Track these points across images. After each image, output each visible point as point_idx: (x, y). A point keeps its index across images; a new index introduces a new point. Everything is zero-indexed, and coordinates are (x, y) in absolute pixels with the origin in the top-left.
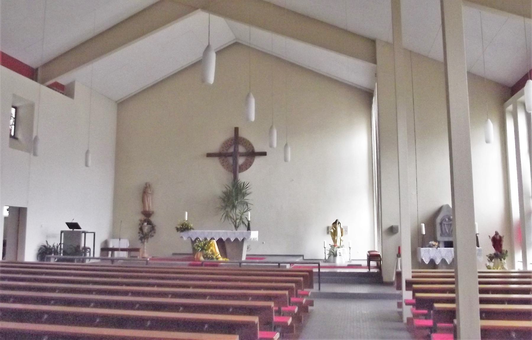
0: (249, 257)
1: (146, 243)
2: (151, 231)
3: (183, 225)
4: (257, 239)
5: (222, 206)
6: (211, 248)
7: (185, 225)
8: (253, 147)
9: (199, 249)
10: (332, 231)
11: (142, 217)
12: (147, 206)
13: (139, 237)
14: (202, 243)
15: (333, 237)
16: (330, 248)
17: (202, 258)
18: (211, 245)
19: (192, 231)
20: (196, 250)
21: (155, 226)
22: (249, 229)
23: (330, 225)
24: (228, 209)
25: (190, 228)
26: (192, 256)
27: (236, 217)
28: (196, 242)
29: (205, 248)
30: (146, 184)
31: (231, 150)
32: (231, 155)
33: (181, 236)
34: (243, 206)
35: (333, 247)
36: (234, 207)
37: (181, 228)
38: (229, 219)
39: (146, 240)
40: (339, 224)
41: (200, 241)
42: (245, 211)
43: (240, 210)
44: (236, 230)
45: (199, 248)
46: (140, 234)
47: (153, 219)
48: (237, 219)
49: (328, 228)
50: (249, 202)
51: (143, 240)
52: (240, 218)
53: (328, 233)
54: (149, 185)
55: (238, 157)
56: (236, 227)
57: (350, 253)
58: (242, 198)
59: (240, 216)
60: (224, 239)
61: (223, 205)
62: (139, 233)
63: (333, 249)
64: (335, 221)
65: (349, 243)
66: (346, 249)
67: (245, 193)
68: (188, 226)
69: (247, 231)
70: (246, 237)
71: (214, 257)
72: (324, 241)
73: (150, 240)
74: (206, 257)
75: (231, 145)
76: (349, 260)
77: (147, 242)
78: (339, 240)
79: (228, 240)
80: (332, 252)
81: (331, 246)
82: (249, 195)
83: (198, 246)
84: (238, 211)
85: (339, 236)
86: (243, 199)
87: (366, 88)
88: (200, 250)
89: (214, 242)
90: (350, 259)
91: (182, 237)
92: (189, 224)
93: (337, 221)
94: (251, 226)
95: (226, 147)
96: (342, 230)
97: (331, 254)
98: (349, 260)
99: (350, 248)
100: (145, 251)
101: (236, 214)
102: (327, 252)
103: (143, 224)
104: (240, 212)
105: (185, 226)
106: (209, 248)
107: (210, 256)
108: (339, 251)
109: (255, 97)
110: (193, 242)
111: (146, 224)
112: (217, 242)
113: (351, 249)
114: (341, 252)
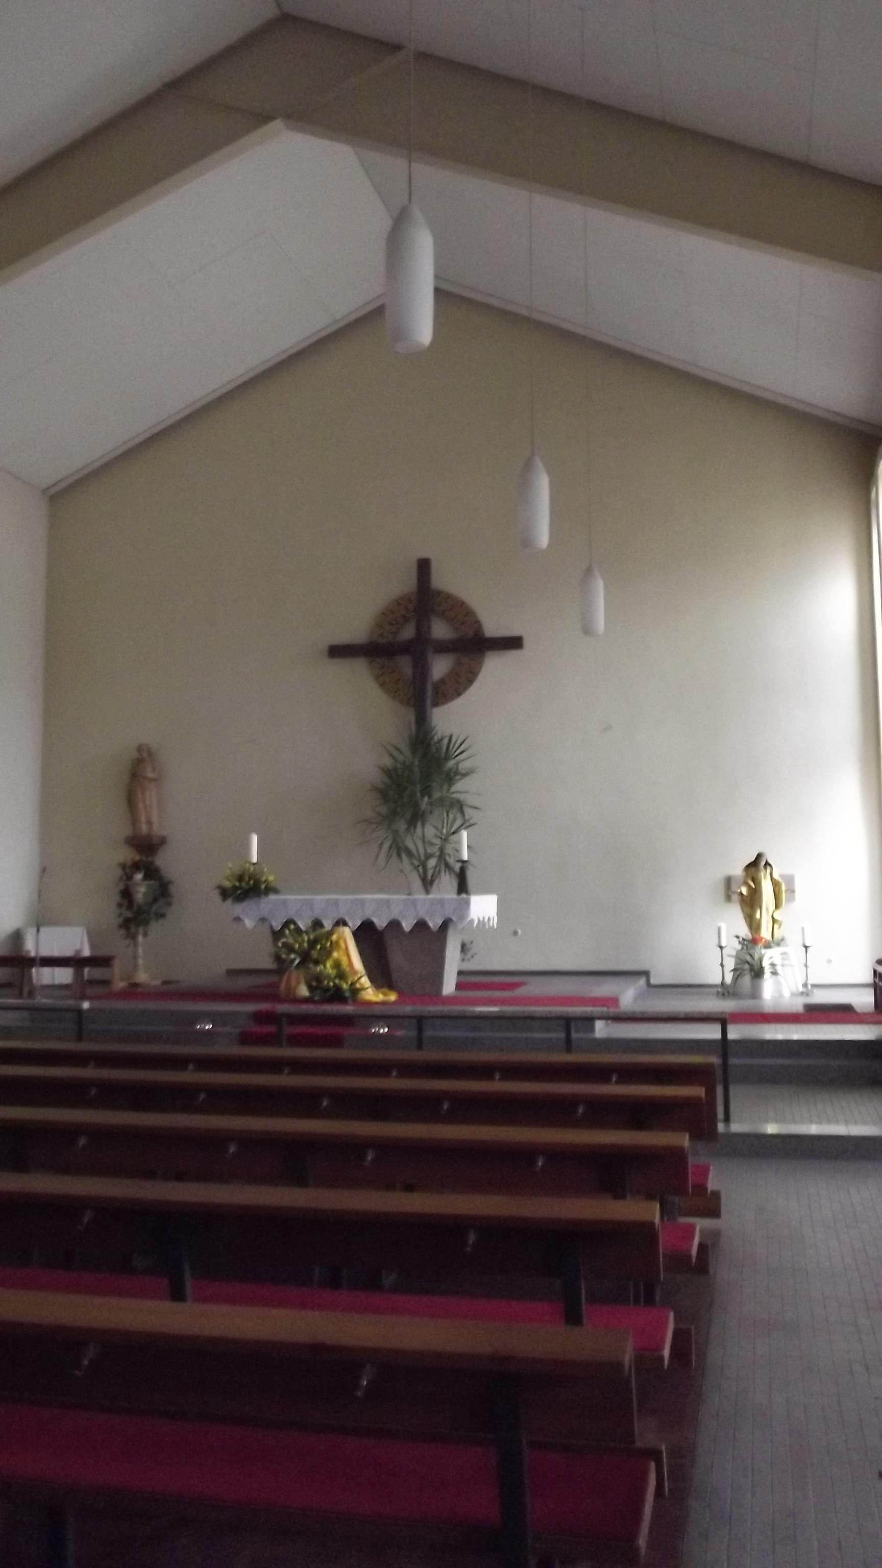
0: (466, 981)
1: (140, 938)
2: (155, 900)
3: (240, 878)
4: (495, 922)
5: (379, 814)
6: (335, 954)
7: (249, 880)
8: (478, 622)
9: (295, 959)
10: (744, 891)
11: (128, 855)
12: (143, 819)
13: (121, 920)
14: (303, 941)
15: (748, 910)
16: (739, 947)
17: (303, 991)
18: (334, 946)
19: (272, 897)
20: (284, 961)
21: (170, 882)
22: (463, 888)
23: (738, 870)
24: (402, 826)
25: (263, 886)
26: (273, 979)
27: (425, 850)
28: (284, 935)
29: (314, 954)
30: (140, 749)
31: (408, 633)
32: (405, 649)
33: (236, 914)
34: (448, 815)
35: (752, 942)
36: (417, 817)
37: (235, 888)
38: (404, 856)
39: (141, 930)
40: (768, 868)
41: (298, 931)
42: (452, 831)
43: (437, 829)
44: (427, 892)
45: (293, 956)
46: (124, 908)
47: (162, 860)
48: (428, 856)
49: (728, 881)
50: (469, 799)
51: (133, 930)
52: (438, 853)
53: (728, 898)
54: (150, 753)
55: (430, 656)
56: (427, 883)
57: (806, 966)
58: (445, 787)
59: (438, 847)
60: (380, 923)
61: (384, 810)
62: (120, 905)
63: (751, 952)
64: (754, 859)
65: (803, 929)
66: (793, 949)
67: (454, 770)
68: (257, 883)
69: (455, 896)
70: (454, 919)
71: (345, 986)
72: (719, 924)
73: (155, 927)
74: (316, 983)
75: (406, 619)
76: (801, 989)
77: (145, 935)
78: (768, 922)
79: (395, 925)
80: (748, 963)
81: (739, 942)
82: (467, 778)
83: (291, 949)
84: (430, 831)
85: (767, 909)
86: (448, 790)
87: (852, 419)
88: (297, 962)
89: (347, 933)
90: (805, 985)
91: (238, 919)
92: (262, 873)
93: (759, 856)
94: (472, 877)
95: (390, 624)
96: (776, 885)
97: (743, 970)
98: (801, 989)
99: (806, 947)
100: (140, 962)
101: (426, 839)
102: (730, 964)
103: (130, 878)
104: (438, 834)
105: (248, 883)
106: (329, 954)
107: (328, 983)
108: (769, 957)
109: (550, 472)
110: (277, 935)
111: (139, 876)
112: (357, 934)
113: (809, 950)
114: (776, 963)
